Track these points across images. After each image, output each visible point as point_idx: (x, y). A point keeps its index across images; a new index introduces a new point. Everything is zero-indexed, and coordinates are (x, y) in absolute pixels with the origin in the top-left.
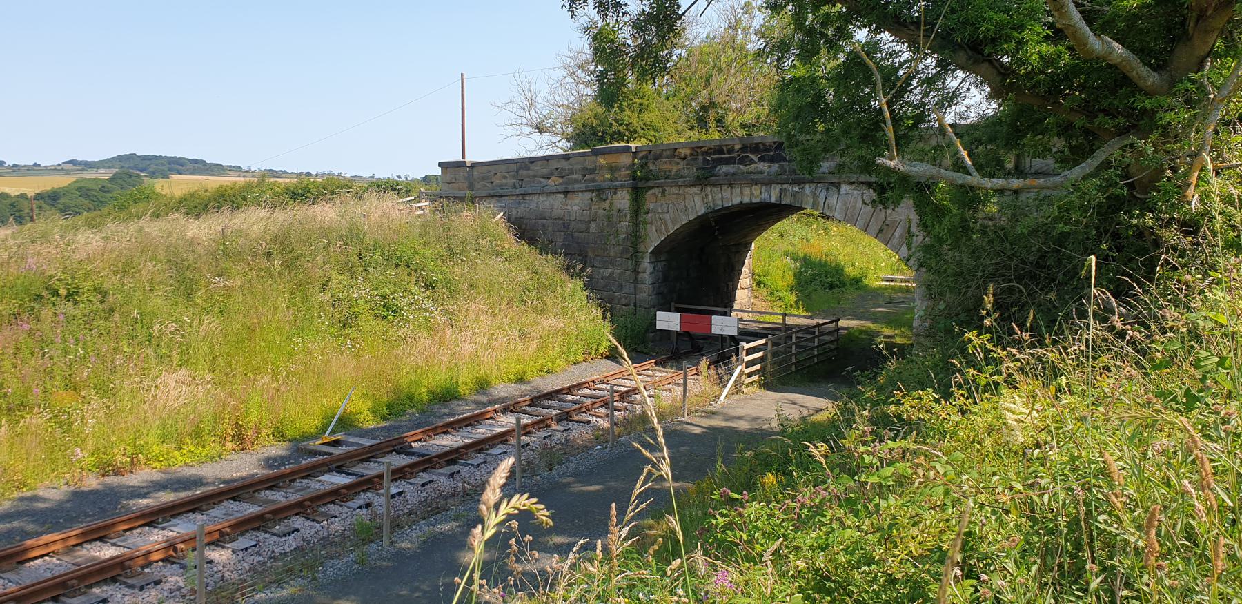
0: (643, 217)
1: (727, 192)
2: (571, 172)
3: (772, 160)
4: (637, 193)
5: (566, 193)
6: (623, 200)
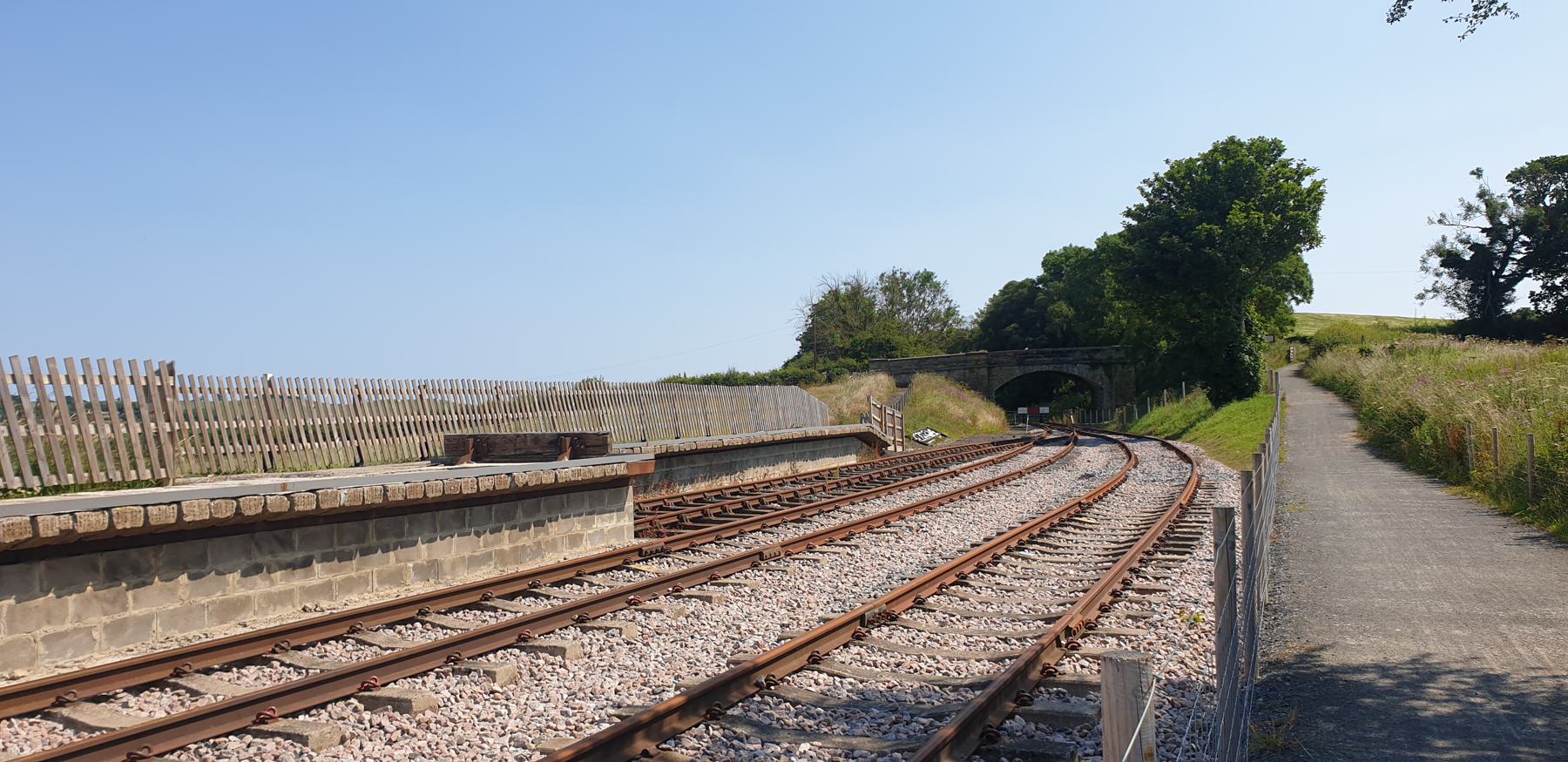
0: (991, 378)
1: (1031, 368)
2: (951, 362)
3: (1049, 357)
4: (989, 369)
5: (949, 371)
6: (984, 372)
